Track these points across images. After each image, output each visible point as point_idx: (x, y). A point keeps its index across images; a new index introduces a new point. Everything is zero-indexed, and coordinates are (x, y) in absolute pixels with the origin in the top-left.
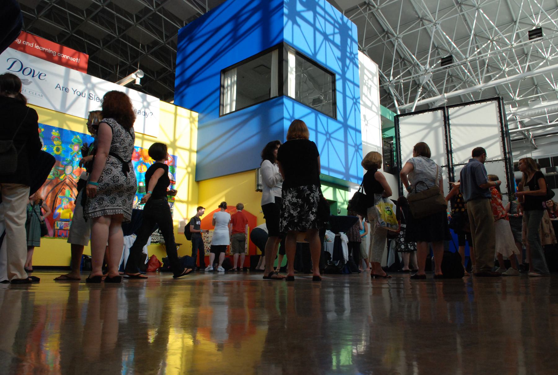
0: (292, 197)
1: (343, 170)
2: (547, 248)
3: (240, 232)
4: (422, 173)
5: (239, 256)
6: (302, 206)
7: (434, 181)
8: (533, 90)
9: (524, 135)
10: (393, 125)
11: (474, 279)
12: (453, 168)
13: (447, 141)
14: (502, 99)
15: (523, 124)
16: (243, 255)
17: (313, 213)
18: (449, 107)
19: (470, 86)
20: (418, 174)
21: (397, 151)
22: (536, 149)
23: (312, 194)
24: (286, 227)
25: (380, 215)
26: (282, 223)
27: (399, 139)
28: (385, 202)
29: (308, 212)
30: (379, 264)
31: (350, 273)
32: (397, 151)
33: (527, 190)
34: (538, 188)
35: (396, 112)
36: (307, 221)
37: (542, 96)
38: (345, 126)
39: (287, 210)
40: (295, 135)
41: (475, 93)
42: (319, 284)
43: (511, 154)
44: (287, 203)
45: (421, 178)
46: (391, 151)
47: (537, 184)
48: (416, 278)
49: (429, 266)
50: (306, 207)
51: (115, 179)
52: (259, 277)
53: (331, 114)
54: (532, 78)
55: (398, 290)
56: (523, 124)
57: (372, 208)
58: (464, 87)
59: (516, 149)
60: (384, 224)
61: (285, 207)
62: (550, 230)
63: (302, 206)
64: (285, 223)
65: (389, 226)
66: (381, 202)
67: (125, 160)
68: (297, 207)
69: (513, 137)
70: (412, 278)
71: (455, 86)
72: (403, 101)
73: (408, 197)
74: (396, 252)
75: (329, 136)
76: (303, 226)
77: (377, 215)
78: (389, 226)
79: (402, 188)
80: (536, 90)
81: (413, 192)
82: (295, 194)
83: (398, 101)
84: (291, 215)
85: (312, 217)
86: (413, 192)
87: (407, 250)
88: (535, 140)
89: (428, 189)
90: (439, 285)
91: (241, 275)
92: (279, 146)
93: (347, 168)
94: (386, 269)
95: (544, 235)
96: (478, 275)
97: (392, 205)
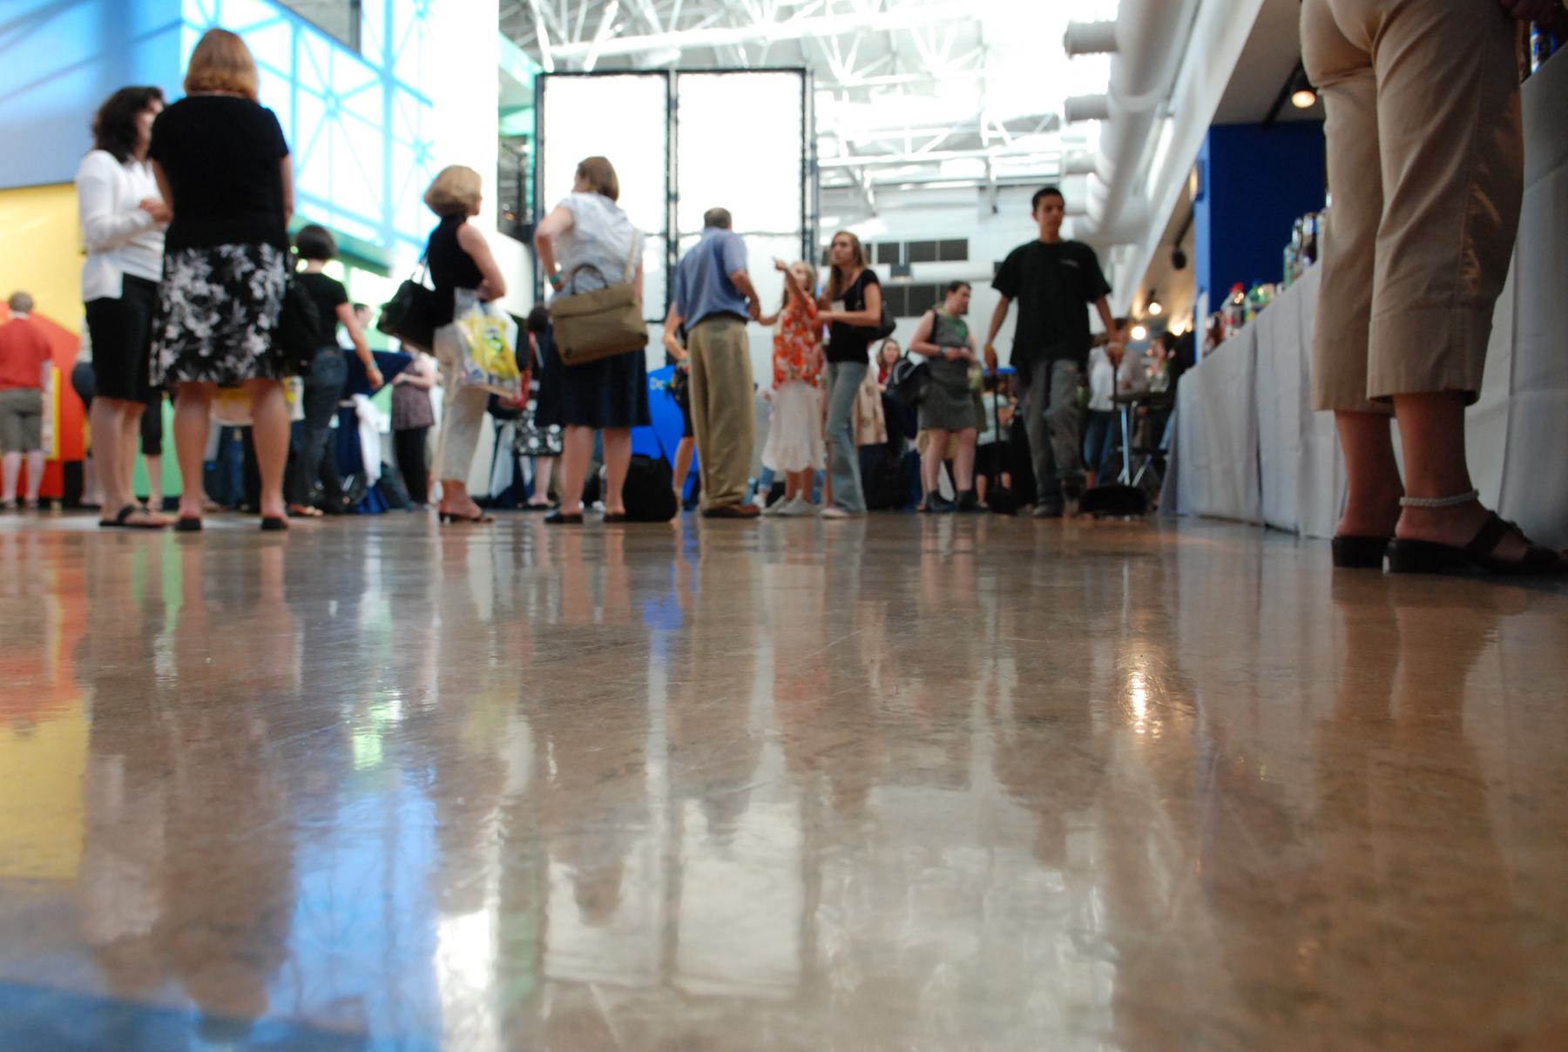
0: (195, 278)
1: (378, 217)
2: (865, 451)
3: (25, 386)
4: (593, 241)
5: (24, 464)
6: (225, 309)
7: (622, 265)
8: (886, 65)
9: (852, 176)
10: (530, 99)
11: (700, 521)
12: (676, 243)
13: (668, 168)
14: (812, 74)
15: (853, 150)
16: (37, 460)
17: (259, 331)
18: (679, 72)
19: (740, 24)
20: (583, 242)
21: (535, 177)
22: (874, 215)
23: (259, 274)
24: (172, 372)
25: (470, 350)
26: (157, 356)
27: (542, 142)
28: (486, 313)
29: (243, 327)
30: (460, 486)
31: (383, 510)
32: (535, 177)
33: (838, 311)
34: (863, 307)
35: (539, 61)
36: (241, 355)
37: (904, 85)
38: (388, 81)
39: (175, 318)
40: (212, 79)
41: (752, 48)
42: (283, 536)
43: (817, 222)
44: (177, 296)
45: (590, 255)
46: (520, 177)
47: (862, 298)
48: (558, 520)
49: (593, 491)
50: (239, 313)
52: (87, 523)
53: (345, 37)
54: (887, 34)
55: (517, 549)
56: (853, 150)
57: (448, 329)
58: (724, 23)
59: (832, 211)
60: (481, 376)
61: (171, 308)
62: (875, 413)
63: (225, 309)
64: (168, 358)
65: (495, 382)
66: (476, 312)
67: (862, 388)
68: (209, 310)
69: (829, 179)
70: (549, 521)
71: (701, 18)
72: (563, 34)
73: (554, 304)
74: (516, 455)
75: (333, 103)
76: (228, 370)
77: (462, 350)
78: (495, 382)
79: (542, 285)
80: (522, 14)
81: (566, 290)
82: (204, 269)
83: (550, 30)
84: (188, 335)
85: (258, 344)
86: (566, 290)
87: (545, 452)
88: (875, 193)
89: (606, 287)
90: (616, 538)
91: (30, 519)
92: (158, 107)
93: (388, 213)
94: (486, 503)
95: (861, 421)
96: (710, 514)
97: (504, 326)
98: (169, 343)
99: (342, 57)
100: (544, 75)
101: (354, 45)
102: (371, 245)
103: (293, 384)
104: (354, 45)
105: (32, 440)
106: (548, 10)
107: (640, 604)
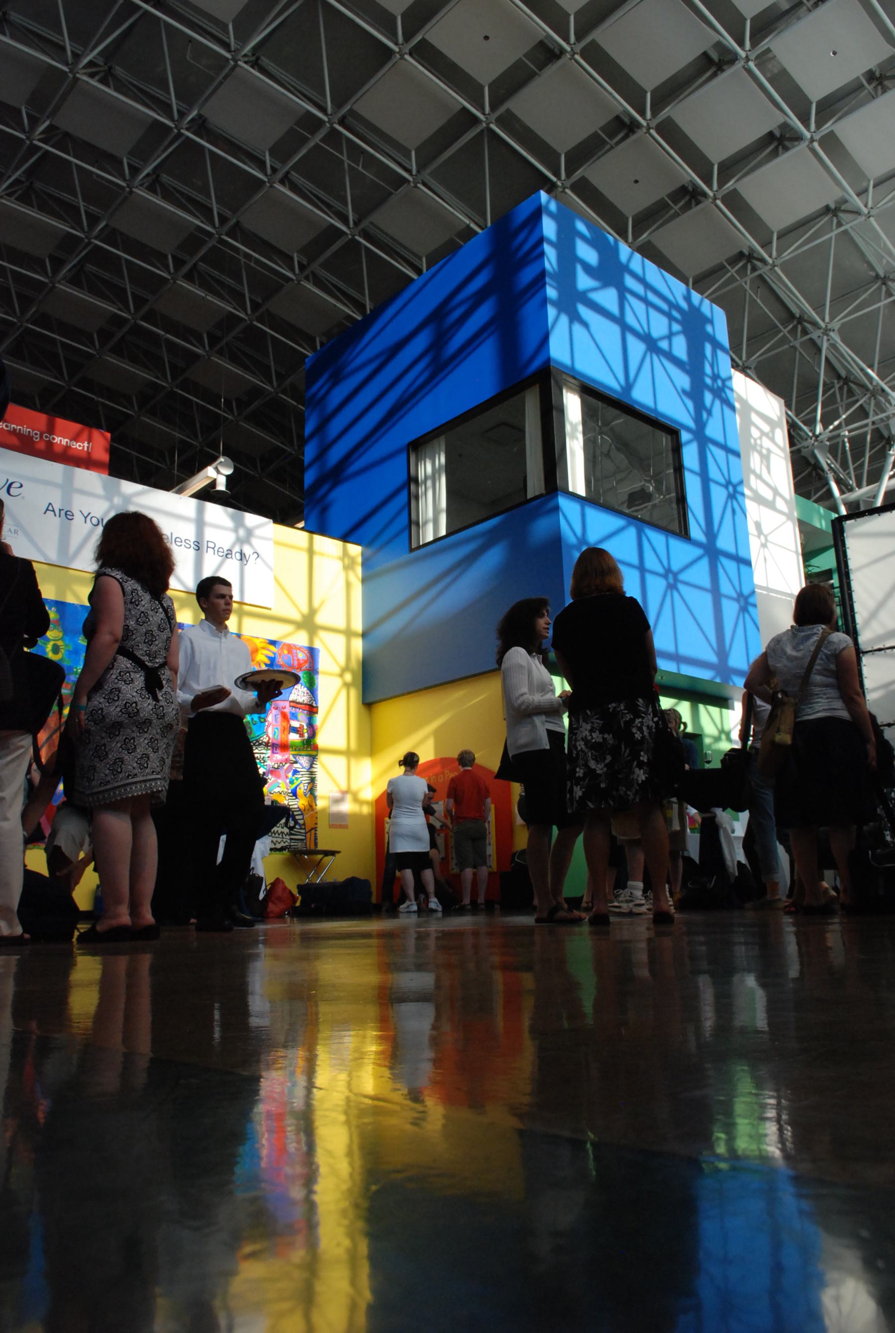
0: (592, 731)
1: (713, 658)
5: (475, 874)
16: (484, 871)
17: (641, 765)
26: (571, 791)
35: (835, 509)
38: (712, 552)
39: (581, 762)
50: (626, 752)
51: (130, 709)
53: (675, 526)
61: (577, 754)
64: (578, 792)
72: (852, 482)
83: (839, 482)
84: (590, 772)
85: (641, 775)
91: (481, 919)
93: (722, 652)
98: (578, 781)
99: (676, 544)
100: (841, 519)
101: (684, 533)
102: (710, 682)
103: (671, 803)
104: (684, 533)
105: (481, 859)
106: (836, 465)
107: (434, 600)
